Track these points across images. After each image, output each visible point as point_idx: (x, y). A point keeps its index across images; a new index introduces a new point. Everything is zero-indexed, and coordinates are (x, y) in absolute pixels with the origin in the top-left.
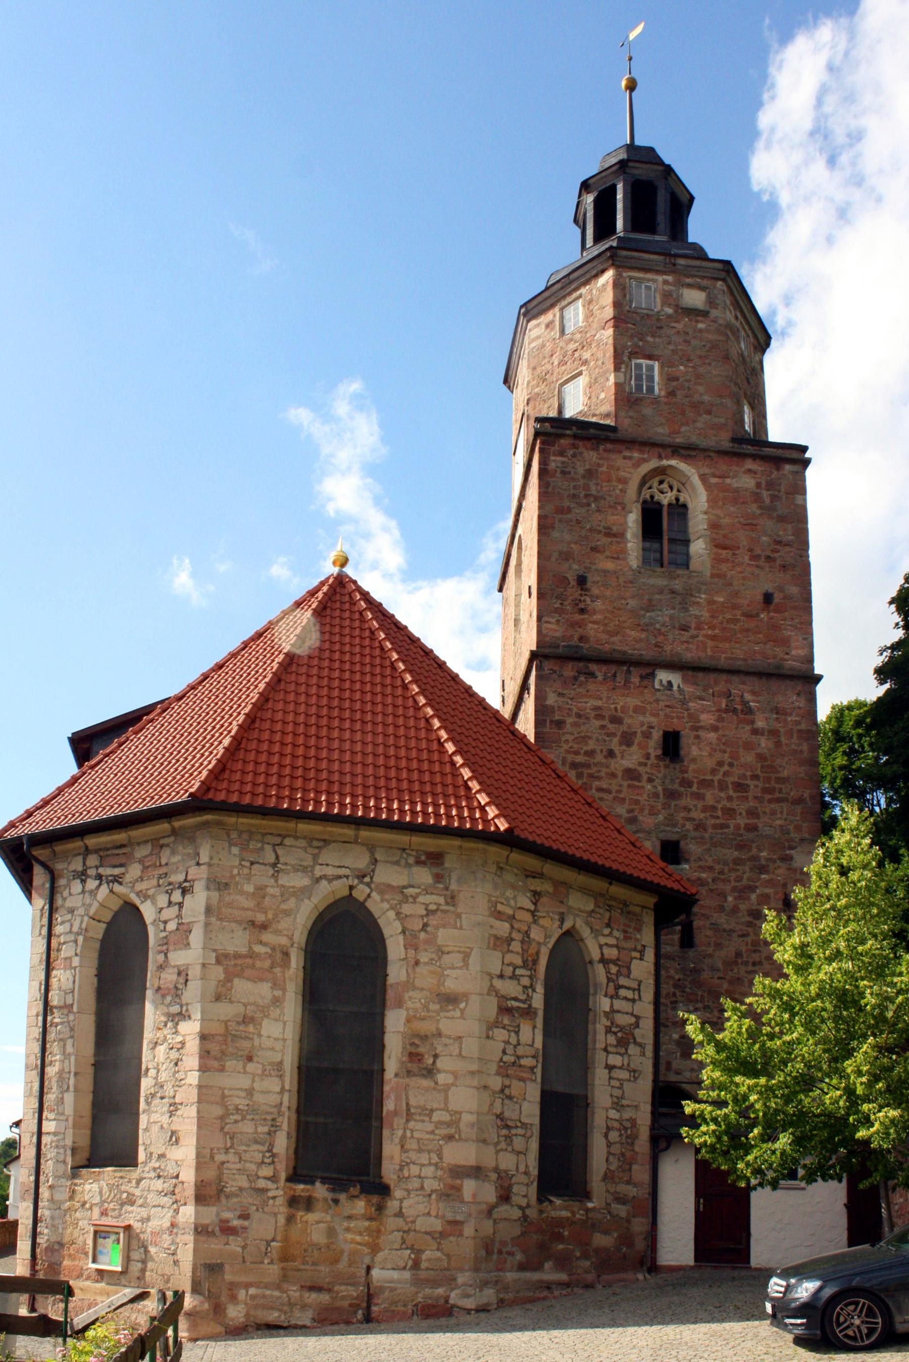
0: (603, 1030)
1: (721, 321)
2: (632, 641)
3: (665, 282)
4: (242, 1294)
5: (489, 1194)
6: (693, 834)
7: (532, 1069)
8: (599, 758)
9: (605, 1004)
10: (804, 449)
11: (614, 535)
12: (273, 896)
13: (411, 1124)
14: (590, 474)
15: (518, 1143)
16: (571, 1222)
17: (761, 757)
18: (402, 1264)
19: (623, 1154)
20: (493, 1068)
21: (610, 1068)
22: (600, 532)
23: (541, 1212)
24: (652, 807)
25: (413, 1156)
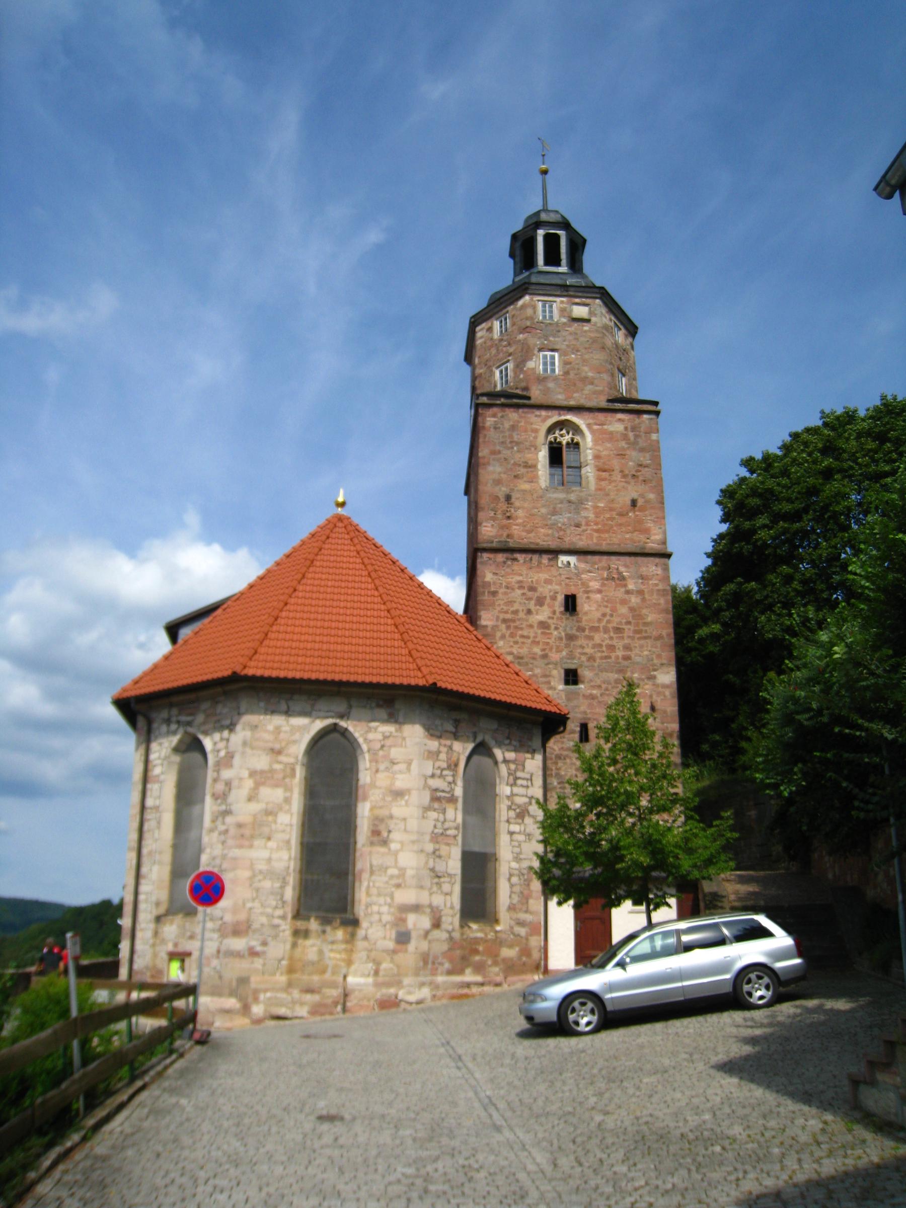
0: (506, 808)
1: (599, 325)
2: (543, 537)
3: (562, 302)
4: (262, 997)
5: (425, 922)
6: (586, 664)
7: (455, 837)
8: (521, 615)
9: (507, 790)
10: (656, 404)
11: (530, 467)
12: (286, 732)
13: (373, 878)
14: (513, 428)
15: (446, 887)
16: (485, 940)
17: (632, 609)
18: (367, 972)
19: (522, 893)
20: (427, 837)
21: (511, 833)
22: (520, 465)
23: (462, 934)
24: (558, 647)
25: (374, 899)
